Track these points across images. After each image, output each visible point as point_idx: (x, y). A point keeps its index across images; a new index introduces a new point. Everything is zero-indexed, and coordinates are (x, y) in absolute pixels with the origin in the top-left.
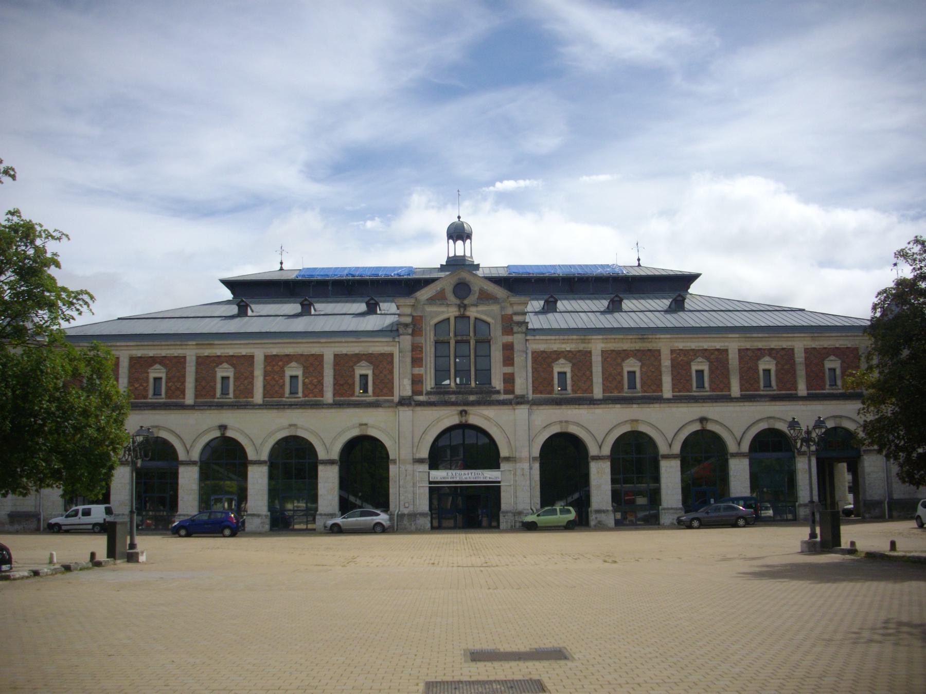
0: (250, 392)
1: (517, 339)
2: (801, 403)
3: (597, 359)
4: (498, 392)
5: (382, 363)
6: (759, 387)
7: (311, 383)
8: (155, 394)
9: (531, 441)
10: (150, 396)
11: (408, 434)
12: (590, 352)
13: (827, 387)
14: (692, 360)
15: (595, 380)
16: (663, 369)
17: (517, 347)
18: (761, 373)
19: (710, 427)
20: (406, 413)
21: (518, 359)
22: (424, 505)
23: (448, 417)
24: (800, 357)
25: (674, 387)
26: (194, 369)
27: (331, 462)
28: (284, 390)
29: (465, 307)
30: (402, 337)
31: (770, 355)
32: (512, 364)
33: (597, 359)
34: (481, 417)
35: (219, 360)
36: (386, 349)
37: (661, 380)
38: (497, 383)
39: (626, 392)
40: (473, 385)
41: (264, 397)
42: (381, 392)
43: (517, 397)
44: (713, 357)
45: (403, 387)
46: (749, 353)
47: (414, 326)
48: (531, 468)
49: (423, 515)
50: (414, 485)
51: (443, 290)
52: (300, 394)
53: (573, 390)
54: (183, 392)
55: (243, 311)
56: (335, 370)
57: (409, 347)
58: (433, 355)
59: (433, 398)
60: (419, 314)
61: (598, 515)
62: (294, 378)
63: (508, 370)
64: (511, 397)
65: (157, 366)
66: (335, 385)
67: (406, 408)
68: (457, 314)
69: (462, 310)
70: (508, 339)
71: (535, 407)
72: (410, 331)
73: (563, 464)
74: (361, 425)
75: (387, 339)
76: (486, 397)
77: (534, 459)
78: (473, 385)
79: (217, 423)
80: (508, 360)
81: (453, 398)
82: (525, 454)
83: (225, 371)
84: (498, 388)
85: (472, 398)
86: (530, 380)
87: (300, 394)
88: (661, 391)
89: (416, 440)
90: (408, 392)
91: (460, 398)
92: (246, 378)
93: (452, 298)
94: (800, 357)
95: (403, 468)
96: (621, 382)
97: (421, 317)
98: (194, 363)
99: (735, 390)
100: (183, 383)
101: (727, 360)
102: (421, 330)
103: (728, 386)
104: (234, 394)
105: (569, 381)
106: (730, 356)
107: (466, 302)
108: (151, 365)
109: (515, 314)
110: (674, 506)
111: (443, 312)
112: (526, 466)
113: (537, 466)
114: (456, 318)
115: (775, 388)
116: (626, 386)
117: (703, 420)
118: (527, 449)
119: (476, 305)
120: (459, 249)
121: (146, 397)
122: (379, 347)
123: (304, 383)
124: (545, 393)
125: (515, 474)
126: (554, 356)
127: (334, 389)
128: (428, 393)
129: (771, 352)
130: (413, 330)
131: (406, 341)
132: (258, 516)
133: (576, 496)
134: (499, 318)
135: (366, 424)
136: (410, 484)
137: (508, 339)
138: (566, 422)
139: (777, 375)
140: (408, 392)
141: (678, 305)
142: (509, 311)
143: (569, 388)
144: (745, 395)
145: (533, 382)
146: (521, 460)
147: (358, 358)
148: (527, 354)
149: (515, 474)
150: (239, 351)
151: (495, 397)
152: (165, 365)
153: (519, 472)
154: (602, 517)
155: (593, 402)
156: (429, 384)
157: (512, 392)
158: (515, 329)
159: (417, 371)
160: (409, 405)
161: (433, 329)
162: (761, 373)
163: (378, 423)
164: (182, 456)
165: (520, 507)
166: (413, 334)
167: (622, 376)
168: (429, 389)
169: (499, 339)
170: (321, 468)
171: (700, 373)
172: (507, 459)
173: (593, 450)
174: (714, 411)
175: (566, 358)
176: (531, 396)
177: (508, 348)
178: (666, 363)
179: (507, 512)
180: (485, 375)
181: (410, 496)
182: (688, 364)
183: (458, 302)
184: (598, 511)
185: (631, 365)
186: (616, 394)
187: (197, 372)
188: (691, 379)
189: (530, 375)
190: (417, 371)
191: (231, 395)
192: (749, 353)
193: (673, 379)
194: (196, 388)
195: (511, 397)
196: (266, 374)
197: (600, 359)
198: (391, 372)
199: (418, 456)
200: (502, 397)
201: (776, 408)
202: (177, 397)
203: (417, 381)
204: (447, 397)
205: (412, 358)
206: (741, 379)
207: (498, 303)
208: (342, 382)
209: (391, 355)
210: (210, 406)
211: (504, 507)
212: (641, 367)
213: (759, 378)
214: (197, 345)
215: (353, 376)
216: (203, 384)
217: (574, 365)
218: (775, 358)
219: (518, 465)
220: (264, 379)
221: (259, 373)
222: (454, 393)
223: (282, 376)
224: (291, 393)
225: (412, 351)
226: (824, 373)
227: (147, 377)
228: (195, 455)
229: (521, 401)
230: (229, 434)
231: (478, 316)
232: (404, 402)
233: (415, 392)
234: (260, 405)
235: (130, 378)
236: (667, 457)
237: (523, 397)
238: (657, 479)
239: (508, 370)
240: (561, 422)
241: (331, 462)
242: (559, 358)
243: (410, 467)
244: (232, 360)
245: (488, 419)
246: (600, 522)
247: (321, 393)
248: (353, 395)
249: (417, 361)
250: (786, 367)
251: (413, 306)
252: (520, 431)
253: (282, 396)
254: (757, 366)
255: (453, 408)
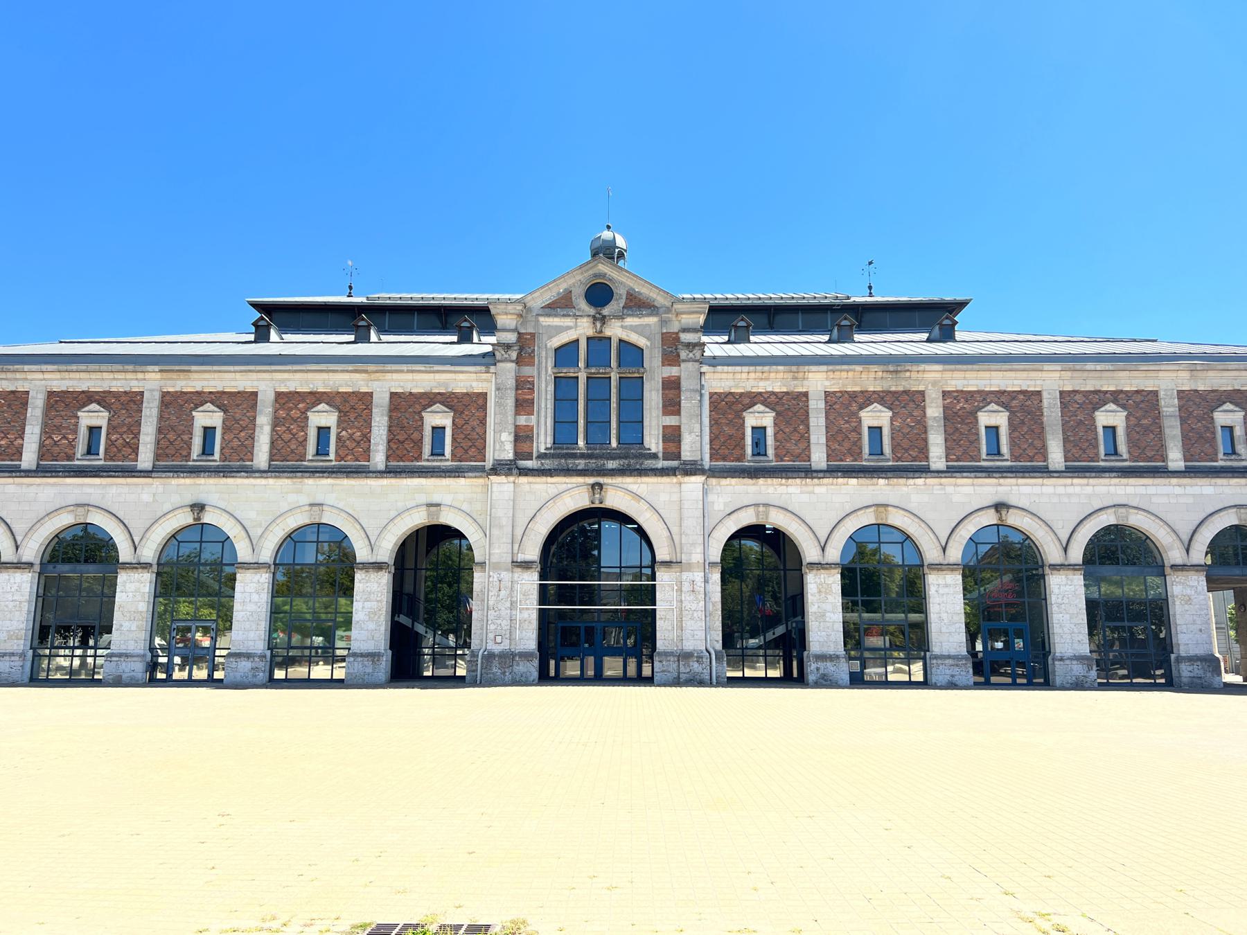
0: (247, 449)
1: (685, 372)
2: (1174, 481)
3: (817, 406)
4: (654, 456)
5: (469, 408)
6: (1097, 454)
7: (351, 437)
8: (89, 452)
9: (707, 535)
10: (79, 456)
11: (506, 520)
12: (806, 394)
13: (1221, 456)
14: (980, 409)
15: (813, 439)
16: (930, 423)
17: (685, 384)
18: (1100, 431)
19: (1013, 519)
20: (502, 486)
21: (688, 403)
22: (528, 639)
23: (570, 495)
24: (1169, 406)
25: (949, 450)
26: (155, 412)
27: (379, 566)
28: (305, 448)
29: (603, 320)
30: (500, 365)
31: (1115, 401)
32: (678, 413)
33: (817, 406)
34: (621, 494)
35: (199, 399)
36: (478, 388)
37: (926, 440)
38: (653, 442)
39: (866, 461)
40: (614, 444)
41: (271, 460)
42: (468, 455)
43: (685, 463)
44: (1014, 403)
45: (500, 445)
46: (1078, 397)
47: (521, 349)
48: (706, 581)
49: (525, 656)
50: (513, 605)
51: (568, 293)
52: (332, 456)
53: (776, 455)
54: (136, 450)
55: (262, 335)
56: (390, 417)
57: (511, 383)
58: (550, 396)
59: (548, 463)
60: (531, 330)
61: (820, 664)
62: (323, 432)
63: (671, 421)
64: (675, 463)
65: (94, 406)
66: (389, 441)
67: (502, 479)
68: (591, 332)
69: (598, 325)
70: (673, 371)
71: (713, 481)
72: (514, 355)
73: (760, 582)
74: (430, 505)
75: (478, 368)
76: (634, 462)
77: (712, 564)
78: (614, 444)
79: (190, 500)
80: (672, 405)
81: (581, 464)
82: (697, 557)
83: (207, 417)
84: (654, 450)
85: (612, 464)
86: (707, 439)
87: (332, 456)
88: (927, 458)
89: (519, 532)
90: (509, 454)
91: (595, 465)
92: (243, 429)
93: (583, 305)
94: (1169, 406)
95: (495, 576)
96: (858, 443)
97: (533, 335)
98: (156, 403)
99: (1056, 457)
100: (137, 436)
101: (1040, 409)
102: (531, 355)
103: (1043, 452)
104: (222, 453)
105: (770, 441)
106: (1045, 403)
107: (606, 311)
108: (84, 405)
109: (685, 330)
110: (953, 652)
111: (569, 328)
112: (698, 576)
113: (716, 576)
114: (588, 339)
115: (1125, 456)
116: (866, 450)
117: (999, 507)
118: (700, 549)
119: (622, 318)
120: (604, 268)
121: (70, 457)
122: (465, 381)
123: (339, 438)
124: (732, 456)
125: (680, 590)
126: (747, 401)
127: (389, 448)
128: (541, 456)
129: (1117, 397)
130: (519, 355)
131: (508, 370)
132: (248, 656)
133: (780, 630)
134: (658, 338)
135: (438, 505)
136: (507, 605)
137: (673, 371)
138: (766, 505)
139: (1128, 435)
140: (509, 454)
141: (947, 335)
142: (674, 327)
143: (771, 452)
144: (953, 467)
145: (711, 441)
146: (689, 567)
147: (429, 399)
148: (701, 395)
149: (680, 590)
150: (212, 383)
151: (649, 463)
152: (107, 407)
153: (686, 587)
154: (829, 667)
155: (809, 473)
156: (543, 441)
157: (678, 456)
158: (684, 354)
159: (522, 420)
160: (508, 473)
161: (552, 354)
162: (1100, 431)
163: (455, 501)
164: (125, 554)
165: (689, 646)
166: (519, 361)
167: (860, 434)
168: (543, 451)
169: (655, 372)
170: (359, 576)
171: (993, 430)
172: (667, 564)
173: (810, 553)
174: (1020, 491)
175: (765, 403)
176: (707, 463)
177: (672, 387)
178: (934, 411)
179: (666, 654)
180: (633, 421)
181: (505, 624)
182: (973, 414)
183: (592, 311)
184: (822, 657)
185: (876, 416)
186: (848, 462)
187: (161, 418)
188: (978, 440)
189: (707, 430)
190: (522, 420)
191: (217, 456)
192: (1078, 397)
193: (946, 440)
194: (158, 442)
195: (675, 463)
196: (276, 422)
197: (822, 405)
198: (483, 422)
199: (520, 557)
200: (661, 464)
201: (1130, 490)
202: (125, 458)
203: (522, 437)
204: (571, 463)
205: (517, 400)
206: (1066, 440)
207: (657, 314)
208: (401, 438)
209: (484, 396)
210: (177, 471)
211: (660, 645)
212: (892, 419)
213: (1096, 439)
214: (161, 371)
215: (420, 428)
216: (171, 436)
217: (778, 414)
218: (1124, 407)
219: (685, 575)
220: (273, 430)
221: (264, 422)
222: (583, 456)
223: (304, 427)
224: (317, 454)
225: (517, 389)
226: (1214, 433)
227: (76, 425)
228: (149, 553)
229: (691, 469)
230: (207, 518)
231: (624, 335)
232: (500, 468)
233: (519, 455)
234: (264, 472)
235: (45, 425)
236: (938, 567)
237: (694, 463)
238: (920, 606)
239: (671, 421)
240: (757, 505)
241: (379, 566)
242: (755, 404)
243: (506, 575)
244: (220, 399)
245: (638, 497)
246: (824, 677)
247: (367, 454)
248: (419, 458)
249: (524, 405)
250: (1144, 422)
251: (521, 316)
252: (685, 521)
253: (302, 457)
254: (1093, 420)
255: (580, 480)
